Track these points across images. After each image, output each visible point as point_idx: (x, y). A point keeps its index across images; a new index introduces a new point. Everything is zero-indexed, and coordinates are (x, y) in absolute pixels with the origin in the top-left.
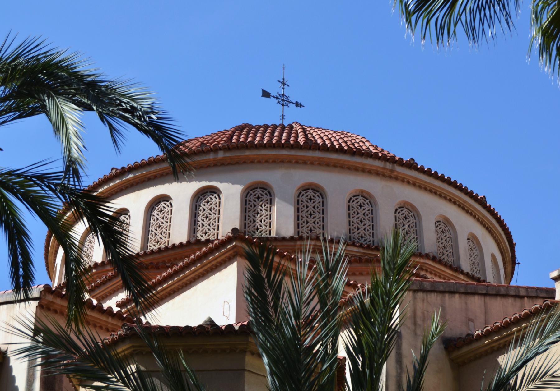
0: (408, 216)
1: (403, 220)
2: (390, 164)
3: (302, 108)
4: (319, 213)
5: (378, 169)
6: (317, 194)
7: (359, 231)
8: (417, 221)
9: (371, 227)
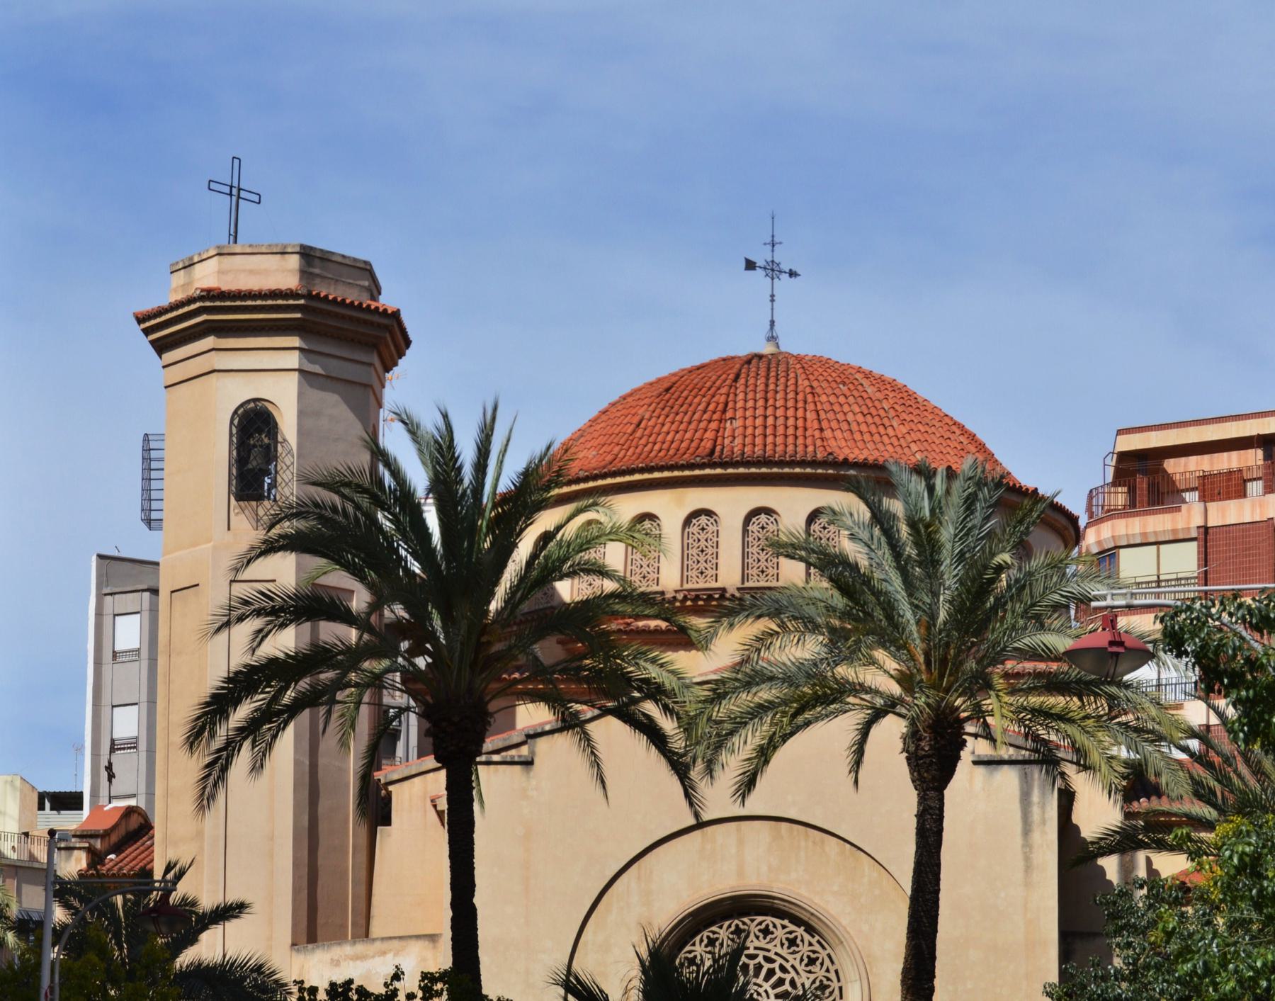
3: (798, 278)
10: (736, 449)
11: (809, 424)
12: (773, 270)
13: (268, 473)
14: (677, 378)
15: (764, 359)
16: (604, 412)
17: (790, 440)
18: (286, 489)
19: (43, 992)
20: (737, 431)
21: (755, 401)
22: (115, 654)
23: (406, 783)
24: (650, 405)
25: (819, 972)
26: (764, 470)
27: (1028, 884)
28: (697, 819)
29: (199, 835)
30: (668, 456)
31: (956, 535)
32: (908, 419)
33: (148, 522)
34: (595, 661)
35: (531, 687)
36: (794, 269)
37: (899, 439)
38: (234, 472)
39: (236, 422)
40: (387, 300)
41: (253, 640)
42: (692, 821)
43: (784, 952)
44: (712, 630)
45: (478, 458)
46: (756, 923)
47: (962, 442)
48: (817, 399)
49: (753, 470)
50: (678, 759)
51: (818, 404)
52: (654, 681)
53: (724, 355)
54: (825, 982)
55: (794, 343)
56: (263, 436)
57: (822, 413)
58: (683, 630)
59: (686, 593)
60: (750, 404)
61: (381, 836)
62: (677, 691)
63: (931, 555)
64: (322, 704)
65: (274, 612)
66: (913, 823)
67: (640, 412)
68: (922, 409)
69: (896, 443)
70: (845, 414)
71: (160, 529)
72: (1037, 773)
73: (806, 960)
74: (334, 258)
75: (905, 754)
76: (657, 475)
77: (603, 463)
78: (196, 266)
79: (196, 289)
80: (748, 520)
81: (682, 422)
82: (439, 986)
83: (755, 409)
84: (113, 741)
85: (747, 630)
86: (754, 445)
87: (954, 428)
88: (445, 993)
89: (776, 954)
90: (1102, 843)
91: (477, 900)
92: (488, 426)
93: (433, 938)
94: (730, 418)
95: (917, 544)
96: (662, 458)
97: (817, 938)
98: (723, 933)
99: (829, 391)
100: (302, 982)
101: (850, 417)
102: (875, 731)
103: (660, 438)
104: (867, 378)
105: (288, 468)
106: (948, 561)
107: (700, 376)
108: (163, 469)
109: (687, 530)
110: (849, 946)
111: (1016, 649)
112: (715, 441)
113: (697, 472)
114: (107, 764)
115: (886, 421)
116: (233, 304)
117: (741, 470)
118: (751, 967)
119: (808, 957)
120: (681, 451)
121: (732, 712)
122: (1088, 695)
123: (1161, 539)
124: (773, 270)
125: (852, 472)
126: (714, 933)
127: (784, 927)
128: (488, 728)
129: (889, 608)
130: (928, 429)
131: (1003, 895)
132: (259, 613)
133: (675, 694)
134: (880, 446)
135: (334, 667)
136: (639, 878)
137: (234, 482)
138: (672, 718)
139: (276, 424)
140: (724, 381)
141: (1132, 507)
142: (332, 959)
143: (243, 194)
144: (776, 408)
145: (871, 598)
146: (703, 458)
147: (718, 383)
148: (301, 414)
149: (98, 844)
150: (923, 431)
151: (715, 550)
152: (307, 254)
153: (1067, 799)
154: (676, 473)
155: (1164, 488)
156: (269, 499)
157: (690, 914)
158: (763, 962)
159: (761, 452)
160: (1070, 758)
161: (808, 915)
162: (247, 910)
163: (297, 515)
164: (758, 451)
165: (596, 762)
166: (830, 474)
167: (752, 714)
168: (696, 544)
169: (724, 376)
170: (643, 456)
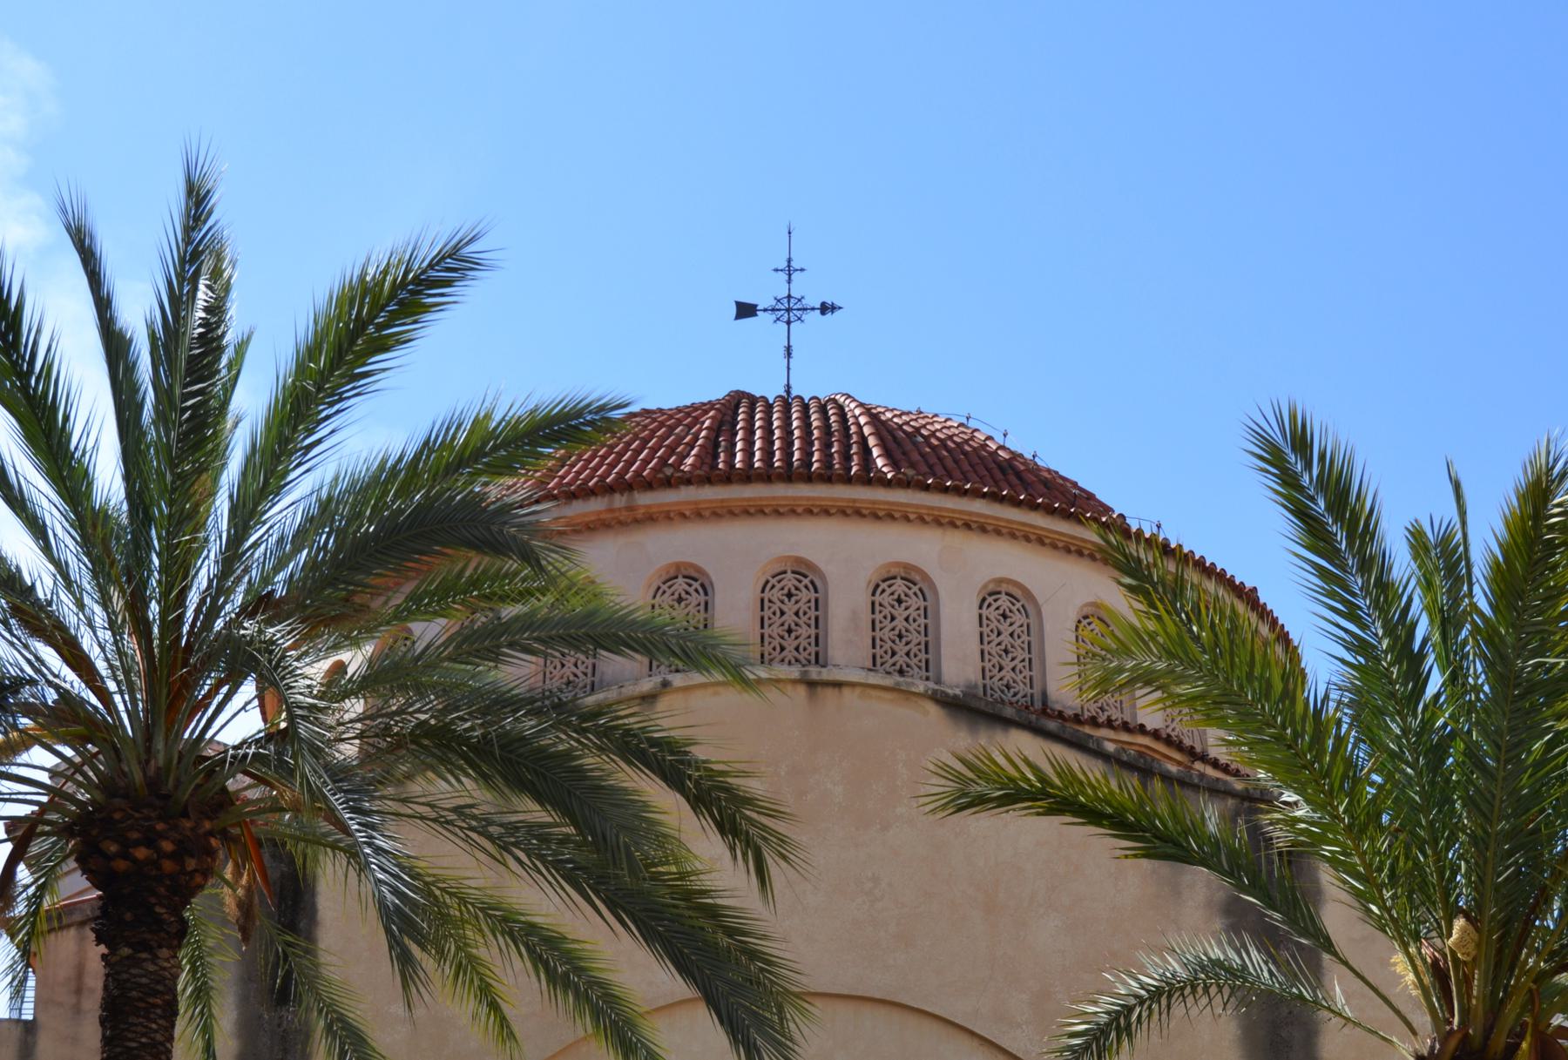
0: (1011, 611)
1: (999, 621)
2: (622, 495)
3: (837, 313)
4: (809, 626)
5: (602, 516)
6: (913, 591)
7: (1003, 673)
8: (1033, 621)
9: (1027, 663)
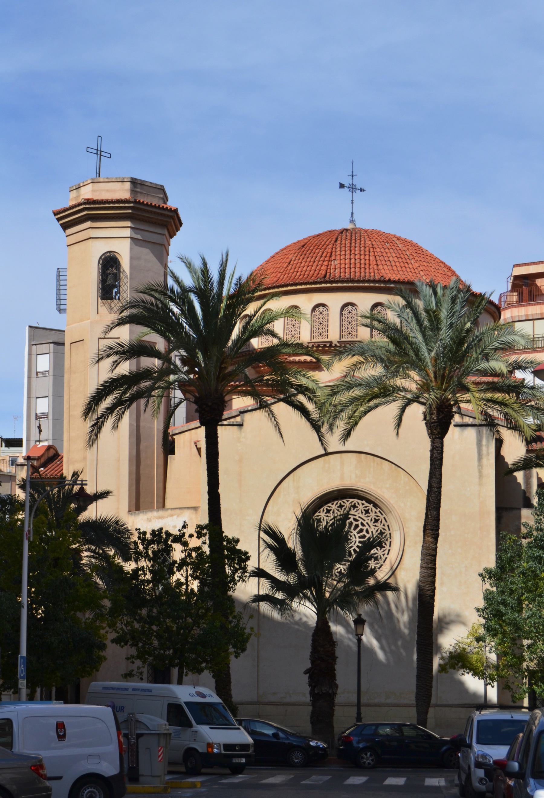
3: (365, 192)
10: (336, 275)
11: (371, 262)
12: (352, 188)
13: (115, 286)
14: (308, 240)
15: (349, 231)
16: (273, 257)
17: (363, 270)
18: (124, 294)
19: (25, 533)
20: (337, 266)
21: (346, 251)
22: (37, 373)
23: (182, 434)
24: (295, 254)
25: (380, 526)
26: (350, 285)
27: (480, 484)
28: (326, 451)
29: (85, 459)
30: (304, 278)
31: (448, 316)
32: (419, 260)
33: (59, 310)
34: (276, 376)
35: (244, 389)
36: (362, 188)
37: (414, 269)
38: (100, 286)
39: (101, 262)
40: (171, 204)
41: (113, 366)
42: (323, 452)
43: (363, 516)
44: (331, 361)
45: (220, 279)
46: (349, 502)
47: (444, 271)
48: (375, 250)
49: (345, 285)
50: (316, 423)
51: (375, 252)
52: (304, 385)
53: (330, 229)
54: (383, 531)
55: (363, 223)
56: (114, 269)
57: (377, 257)
58: (318, 360)
59: (313, 344)
60: (343, 253)
61: (170, 460)
62: (315, 390)
63: (437, 325)
64: (145, 397)
65: (124, 353)
66: (429, 454)
67: (290, 257)
68: (425, 255)
69: (413, 271)
70: (389, 257)
71: (65, 313)
72: (485, 431)
73: (373, 520)
74: (147, 184)
75: (425, 421)
76: (299, 287)
77: (272, 282)
78: (82, 188)
79: (82, 199)
80: (342, 308)
81: (310, 262)
82: (205, 531)
83: (345, 255)
84: (36, 414)
85: (347, 362)
86: (345, 273)
87: (441, 264)
88: (208, 534)
89: (359, 517)
90: (519, 464)
91: (220, 491)
92: (224, 262)
93: (195, 508)
94: (334, 260)
95: (430, 320)
96: (301, 279)
97: (379, 509)
98: (334, 506)
99: (381, 246)
100: (139, 529)
101: (391, 259)
102: (408, 410)
103: (300, 269)
104: (399, 240)
105: (125, 284)
106: (445, 328)
107: (319, 240)
108: (66, 285)
109: (313, 313)
110: (395, 514)
111: (478, 370)
112: (327, 271)
113: (318, 286)
114: (38, 425)
115: (408, 261)
116: (99, 206)
117: (339, 285)
118: (354, 525)
119: (375, 518)
120: (310, 275)
121: (341, 401)
122: (512, 393)
123: (535, 318)
124: (352, 188)
125: (392, 285)
126: (329, 507)
127: (363, 504)
128: (225, 408)
129: (417, 351)
130: (428, 265)
131: (468, 489)
132: (117, 353)
133: (315, 392)
134: (406, 273)
135: (151, 379)
136: (294, 481)
137: (100, 291)
138: (312, 403)
139: (120, 263)
140: (330, 242)
141: (521, 301)
142: (147, 518)
143: (103, 154)
144: (355, 255)
145: (409, 346)
146: (321, 279)
147: (327, 243)
148: (132, 258)
149: (35, 463)
150: (426, 265)
151: (327, 323)
152: (134, 182)
153: (499, 443)
154: (308, 286)
155: (536, 293)
156: (116, 299)
157: (318, 498)
158: (353, 521)
159: (349, 276)
160: (503, 425)
161: (375, 499)
162: (110, 494)
163: (132, 307)
164: (347, 275)
165: (277, 424)
166: (382, 286)
167: (351, 402)
168: (291, 323)
169: (330, 239)
170: (292, 278)
